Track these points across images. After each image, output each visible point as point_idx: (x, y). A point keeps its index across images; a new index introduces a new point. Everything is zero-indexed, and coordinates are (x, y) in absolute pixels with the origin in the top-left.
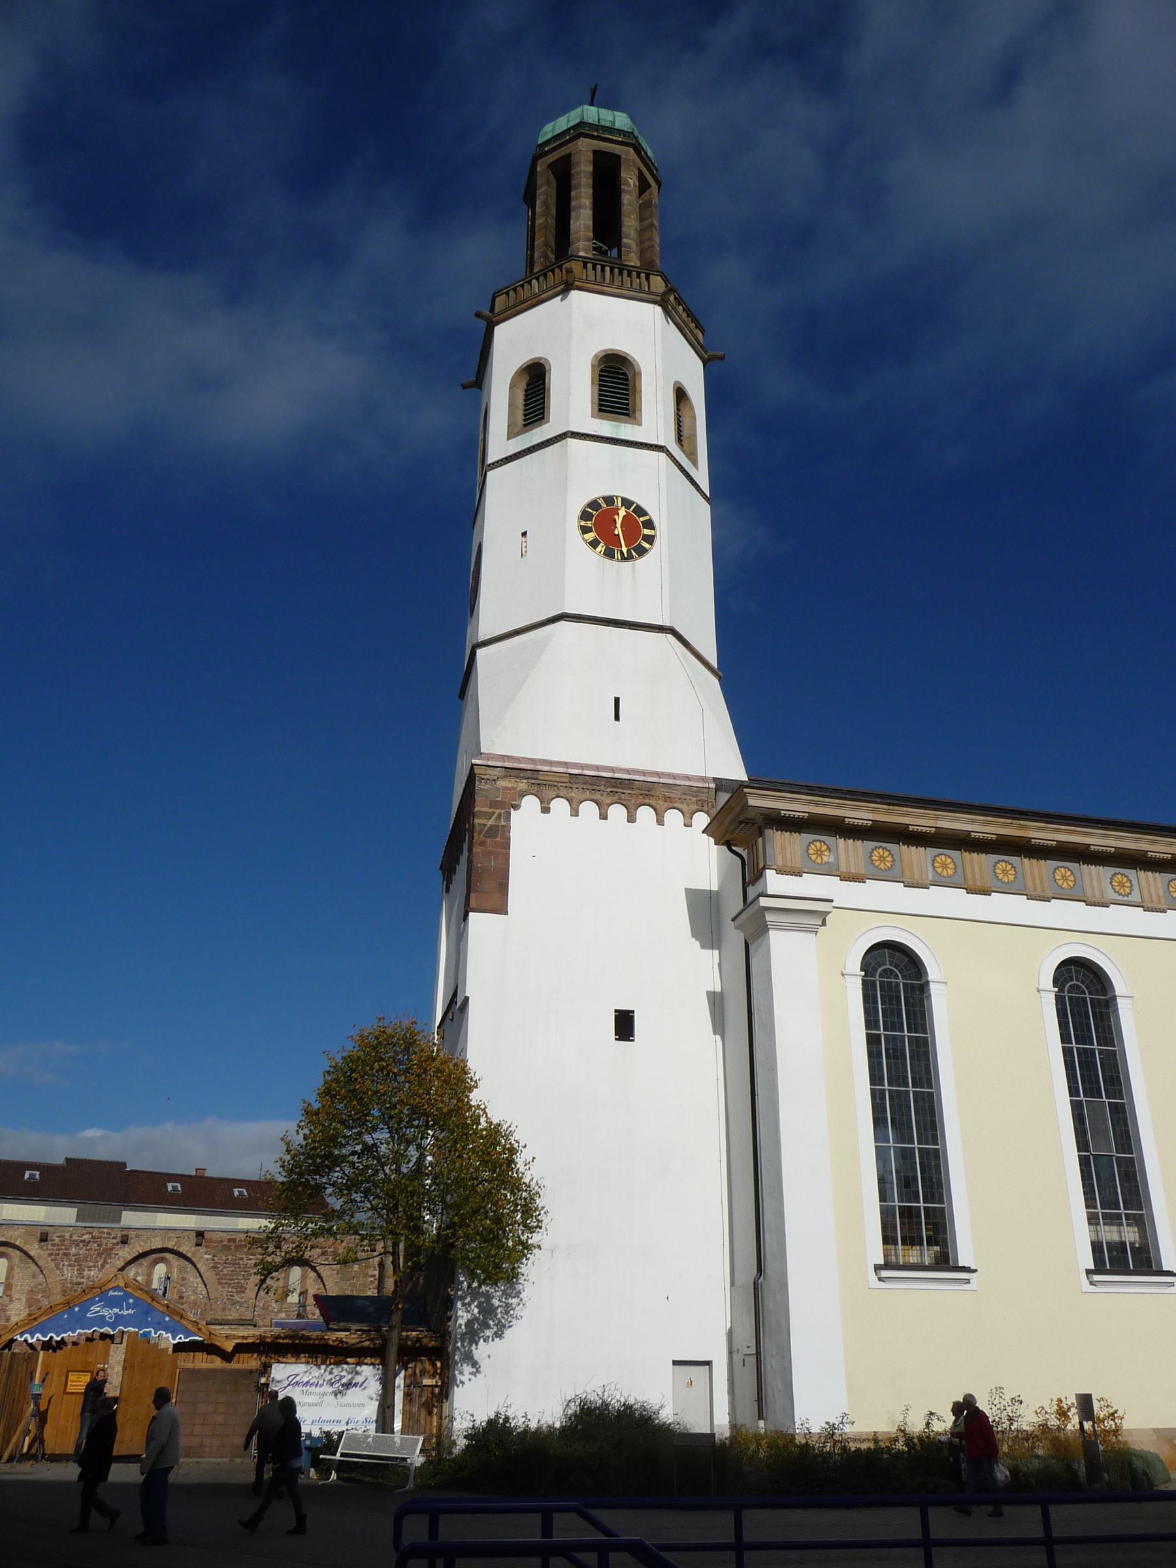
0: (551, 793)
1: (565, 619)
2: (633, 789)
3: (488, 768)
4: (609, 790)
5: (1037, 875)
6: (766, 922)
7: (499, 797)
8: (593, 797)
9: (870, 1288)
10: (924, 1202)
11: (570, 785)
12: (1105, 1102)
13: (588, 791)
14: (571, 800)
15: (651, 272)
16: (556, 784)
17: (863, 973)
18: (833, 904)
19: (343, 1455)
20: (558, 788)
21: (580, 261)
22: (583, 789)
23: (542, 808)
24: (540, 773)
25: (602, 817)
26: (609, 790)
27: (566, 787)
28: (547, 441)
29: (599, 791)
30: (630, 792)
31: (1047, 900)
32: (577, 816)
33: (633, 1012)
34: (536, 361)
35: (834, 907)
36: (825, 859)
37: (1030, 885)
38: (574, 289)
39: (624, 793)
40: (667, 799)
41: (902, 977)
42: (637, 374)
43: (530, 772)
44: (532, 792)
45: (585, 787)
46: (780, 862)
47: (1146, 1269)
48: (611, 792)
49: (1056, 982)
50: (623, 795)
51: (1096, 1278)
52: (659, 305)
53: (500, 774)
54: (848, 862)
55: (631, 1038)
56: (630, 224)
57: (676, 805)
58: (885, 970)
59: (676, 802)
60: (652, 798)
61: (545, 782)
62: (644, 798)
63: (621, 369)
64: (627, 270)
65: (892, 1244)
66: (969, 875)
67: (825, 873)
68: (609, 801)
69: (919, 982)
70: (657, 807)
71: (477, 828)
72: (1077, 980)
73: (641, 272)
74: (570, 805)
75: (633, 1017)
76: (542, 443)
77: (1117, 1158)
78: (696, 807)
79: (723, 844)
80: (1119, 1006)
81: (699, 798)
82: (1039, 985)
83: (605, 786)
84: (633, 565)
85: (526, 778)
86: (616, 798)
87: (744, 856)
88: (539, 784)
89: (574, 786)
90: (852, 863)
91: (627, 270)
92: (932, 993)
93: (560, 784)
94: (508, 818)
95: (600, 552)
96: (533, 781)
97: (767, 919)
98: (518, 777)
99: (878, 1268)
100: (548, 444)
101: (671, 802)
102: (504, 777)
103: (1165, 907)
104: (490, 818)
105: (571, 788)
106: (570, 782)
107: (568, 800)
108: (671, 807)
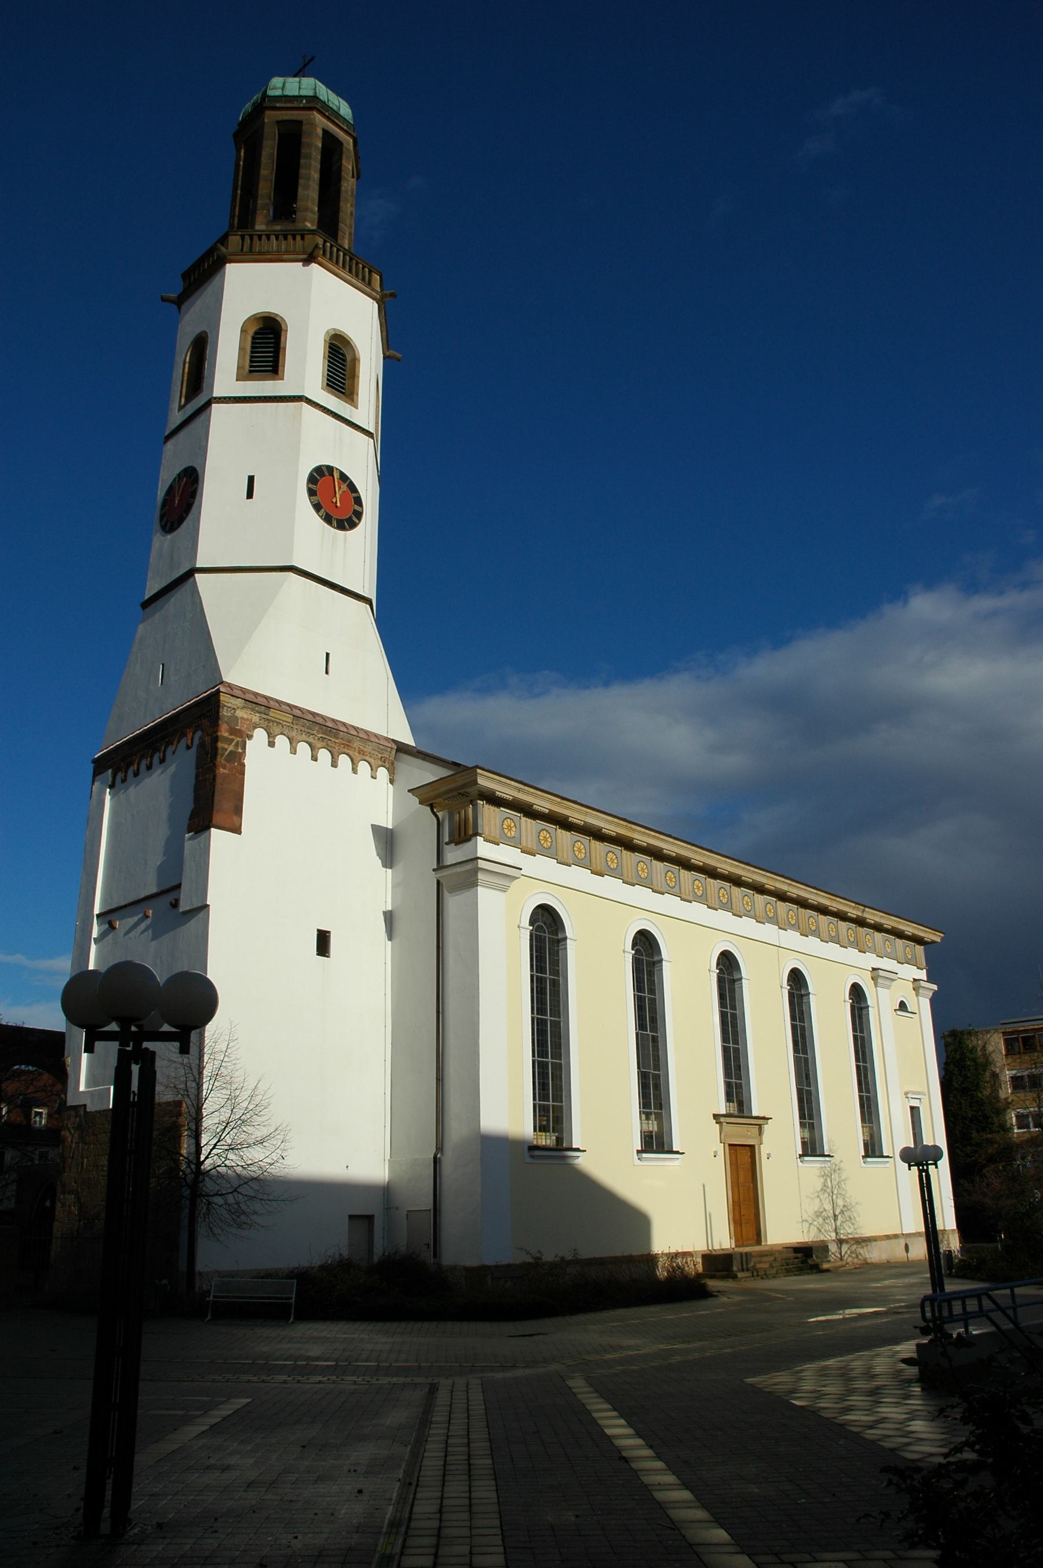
0: (276, 729)
1: (293, 571)
2: (337, 738)
3: (232, 698)
4: (320, 735)
5: (629, 864)
6: (478, 879)
7: (238, 726)
8: (308, 739)
9: (634, 1165)
10: (553, 1102)
11: (292, 726)
12: (648, 1034)
13: (304, 733)
14: (292, 739)
15: (374, 270)
16: (281, 722)
17: (633, 952)
18: (522, 872)
19: (215, 1297)
20: (283, 726)
21: (322, 238)
22: (301, 731)
23: (269, 742)
24: (272, 710)
25: (313, 759)
26: (320, 735)
27: (288, 726)
28: (281, 397)
29: (312, 735)
30: (334, 740)
31: (633, 885)
32: (295, 754)
33: (329, 932)
34: (272, 316)
35: (522, 875)
36: (513, 833)
37: (625, 875)
38: (315, 263)
39: (330, 740)
40: (361, 752)
41: (548, 932)
42: (355, 360)
43: (264, 707)
44: (263, 726)
45: (303, 729)
46: (486, 832)
47: (661, 1149)
48: (321, 737)
49: (531, 923)
50: (329, 741)
51: (644, 1155)
52: (377, 303)
53: (240, 705)
54: (527, 842)
55: (327, 955)
56: (347, 208)
57: (367, 758)
58: (538, 926)
59: (366, 755)
60: (350, 748)
61: (273, 719)
62: (344, 747)
63: (341, 349)
64: (356, 260)
65: (543, 1132)
66: (593, 860)
67: (673, 893)
68: (320, 746)
69: (652, 960)
70: (354, 757)
71: (220, 752)
72: (542, 922)
73: (347, 255)
74: (291, 743)
75: (329, 936)
76: (275, 397)
77: (653, 1074)
78: (380, 763)
79: (427, 805)
80: (664, 967)
81: (383, 755)
82: (520, 923)
83: (318, 731)
84: (345, 535)
85: (260, 713)
86: (324, 744)
87: (439, 816)
88: (268, 720)
89: (295, 727)
90: (529, 842)
91: (356, 260)
92: (568, 947)
93: (285, 723)
94: (244, 748)
95: (322, 516)
96: (264, 716)
97: (479, 878)
98: (253, 710)
99: (638, 1152)
100: (285, 400)
101: (364, 755)
102: (243, 708)
103: (692, 899)
104: (230, 744)
105: (292, 728)
106: (292, 723)
107: (289, 738)
108: (363, 759)
